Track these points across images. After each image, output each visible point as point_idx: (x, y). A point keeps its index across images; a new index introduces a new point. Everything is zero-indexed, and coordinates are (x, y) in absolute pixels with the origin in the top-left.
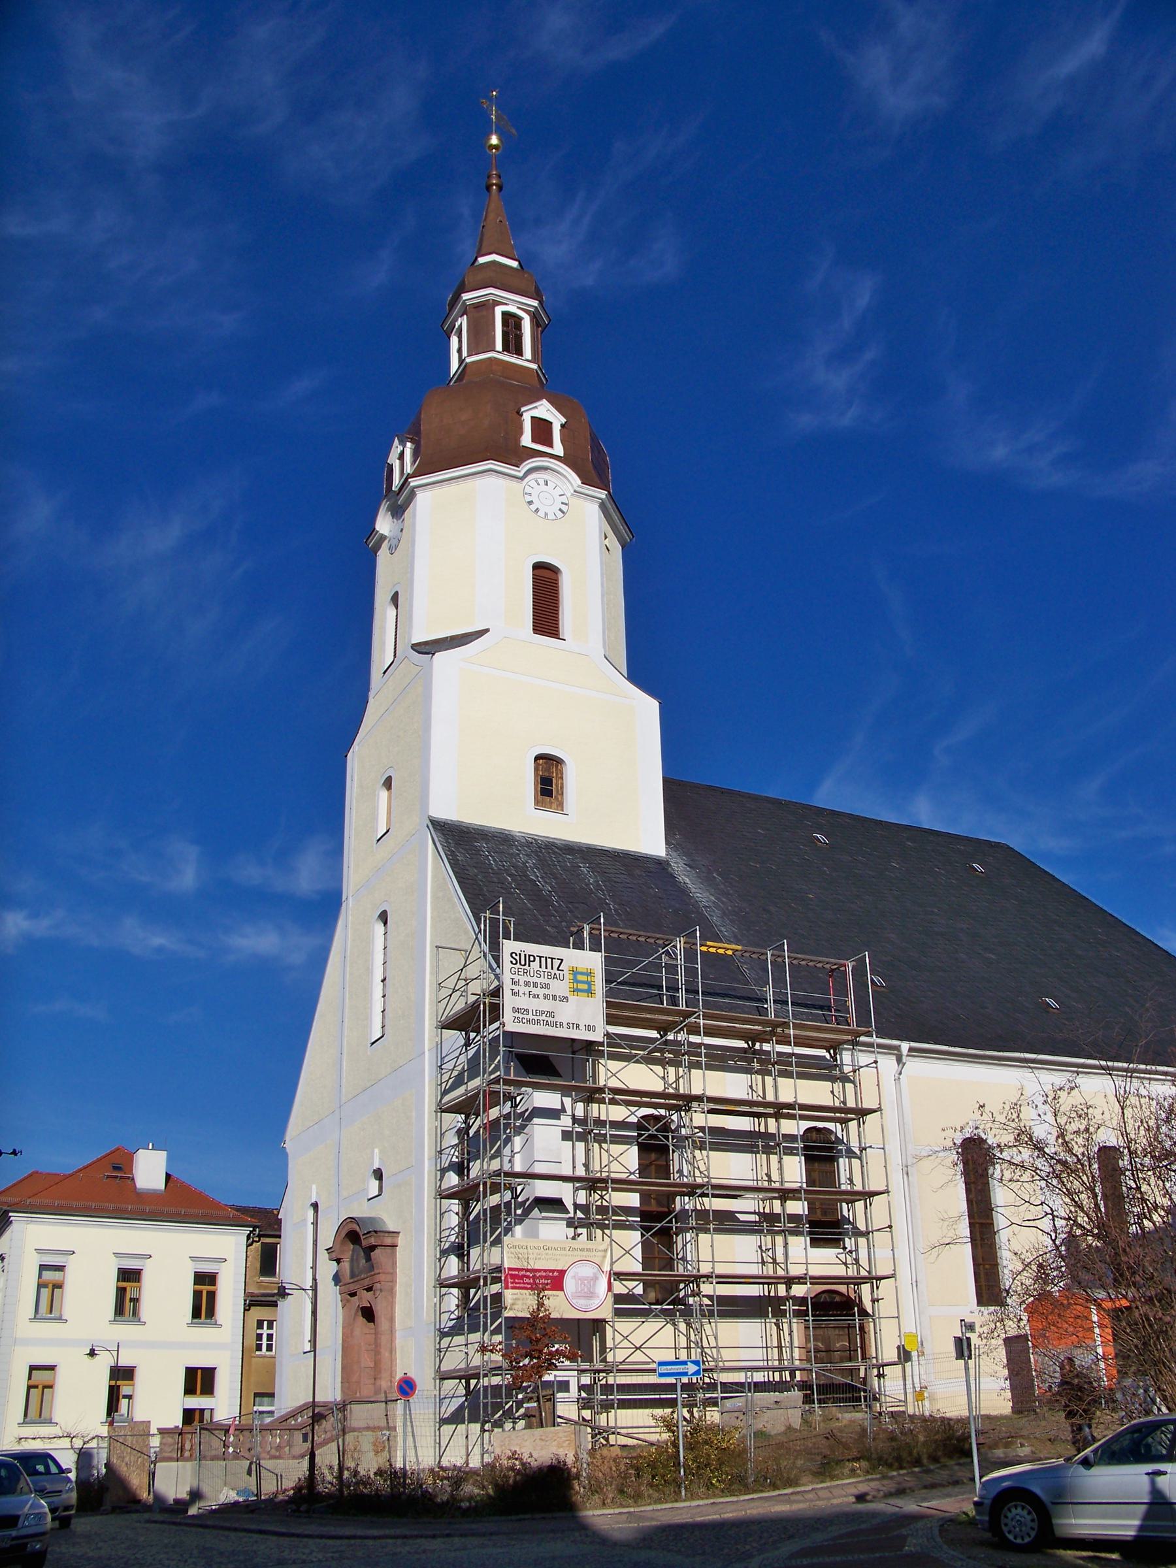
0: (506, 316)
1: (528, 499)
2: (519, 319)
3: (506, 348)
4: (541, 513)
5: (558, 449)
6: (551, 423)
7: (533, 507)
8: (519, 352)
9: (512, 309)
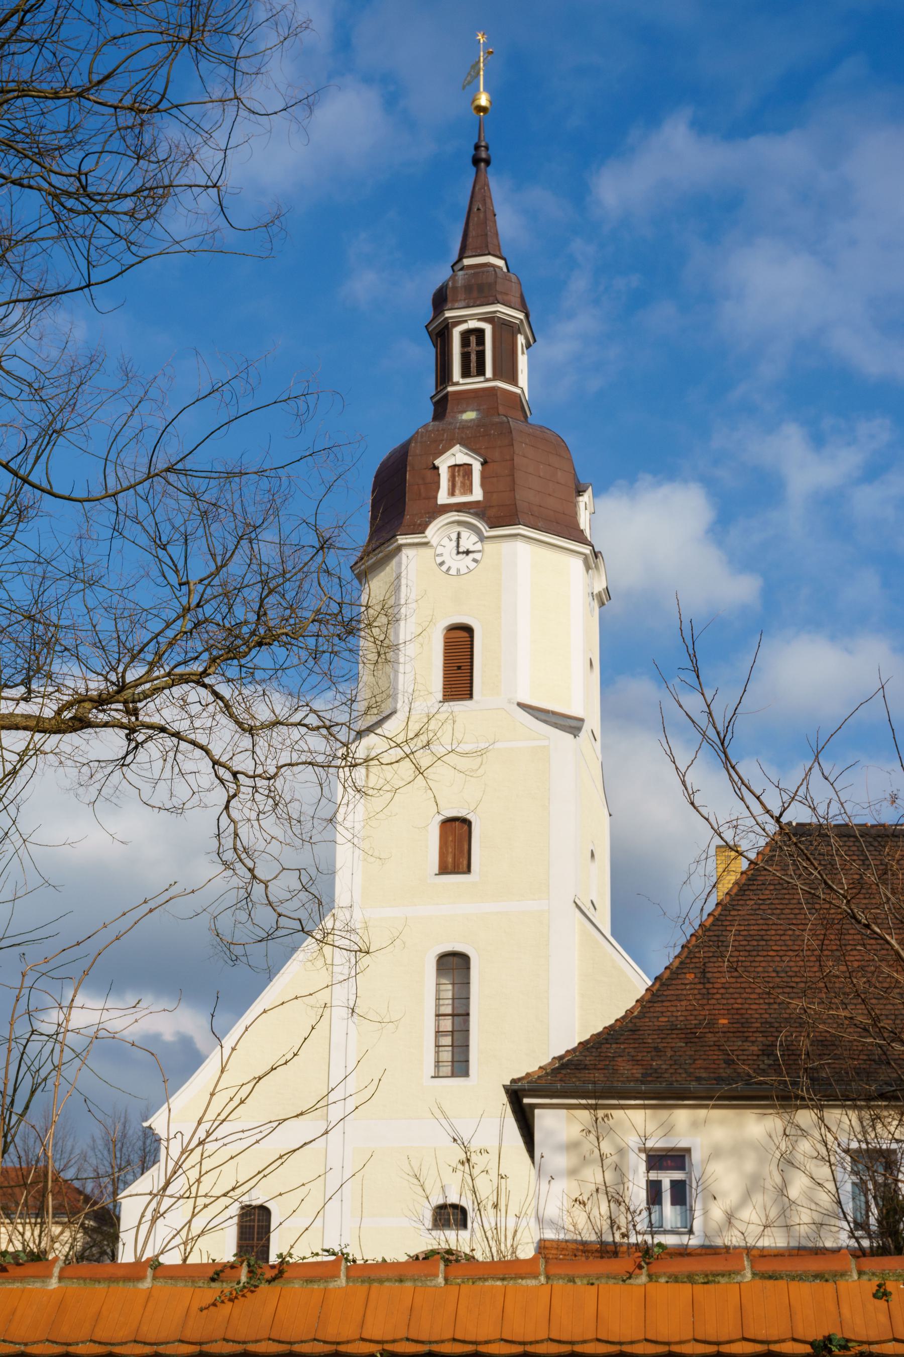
0: (466, 336)
1: (439, 560)
2: (480, 333)
3: (466, 373)
4: (453, 571)
5: (477, 494)
6: (471, 465)
7: (444, 568)
8: (481, 371)
9: (473, 324)
